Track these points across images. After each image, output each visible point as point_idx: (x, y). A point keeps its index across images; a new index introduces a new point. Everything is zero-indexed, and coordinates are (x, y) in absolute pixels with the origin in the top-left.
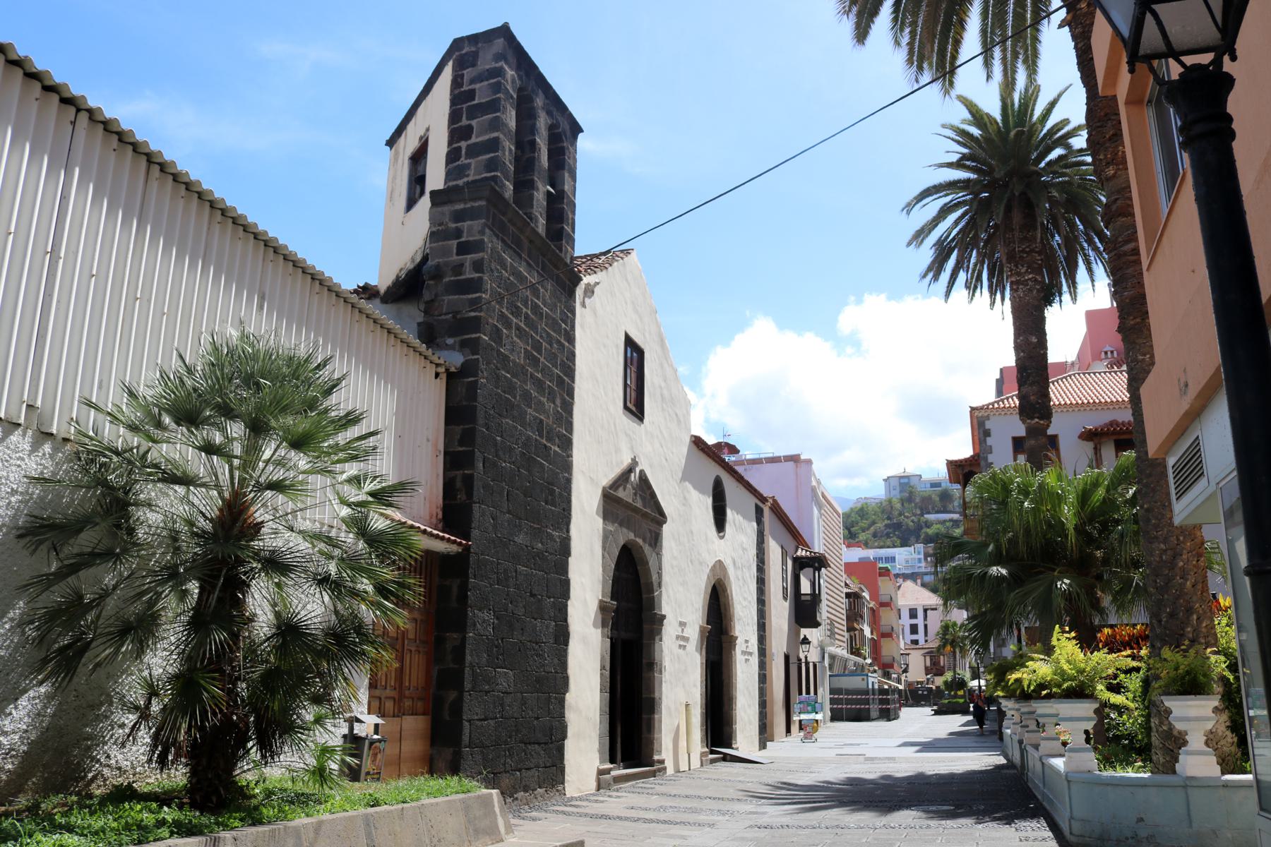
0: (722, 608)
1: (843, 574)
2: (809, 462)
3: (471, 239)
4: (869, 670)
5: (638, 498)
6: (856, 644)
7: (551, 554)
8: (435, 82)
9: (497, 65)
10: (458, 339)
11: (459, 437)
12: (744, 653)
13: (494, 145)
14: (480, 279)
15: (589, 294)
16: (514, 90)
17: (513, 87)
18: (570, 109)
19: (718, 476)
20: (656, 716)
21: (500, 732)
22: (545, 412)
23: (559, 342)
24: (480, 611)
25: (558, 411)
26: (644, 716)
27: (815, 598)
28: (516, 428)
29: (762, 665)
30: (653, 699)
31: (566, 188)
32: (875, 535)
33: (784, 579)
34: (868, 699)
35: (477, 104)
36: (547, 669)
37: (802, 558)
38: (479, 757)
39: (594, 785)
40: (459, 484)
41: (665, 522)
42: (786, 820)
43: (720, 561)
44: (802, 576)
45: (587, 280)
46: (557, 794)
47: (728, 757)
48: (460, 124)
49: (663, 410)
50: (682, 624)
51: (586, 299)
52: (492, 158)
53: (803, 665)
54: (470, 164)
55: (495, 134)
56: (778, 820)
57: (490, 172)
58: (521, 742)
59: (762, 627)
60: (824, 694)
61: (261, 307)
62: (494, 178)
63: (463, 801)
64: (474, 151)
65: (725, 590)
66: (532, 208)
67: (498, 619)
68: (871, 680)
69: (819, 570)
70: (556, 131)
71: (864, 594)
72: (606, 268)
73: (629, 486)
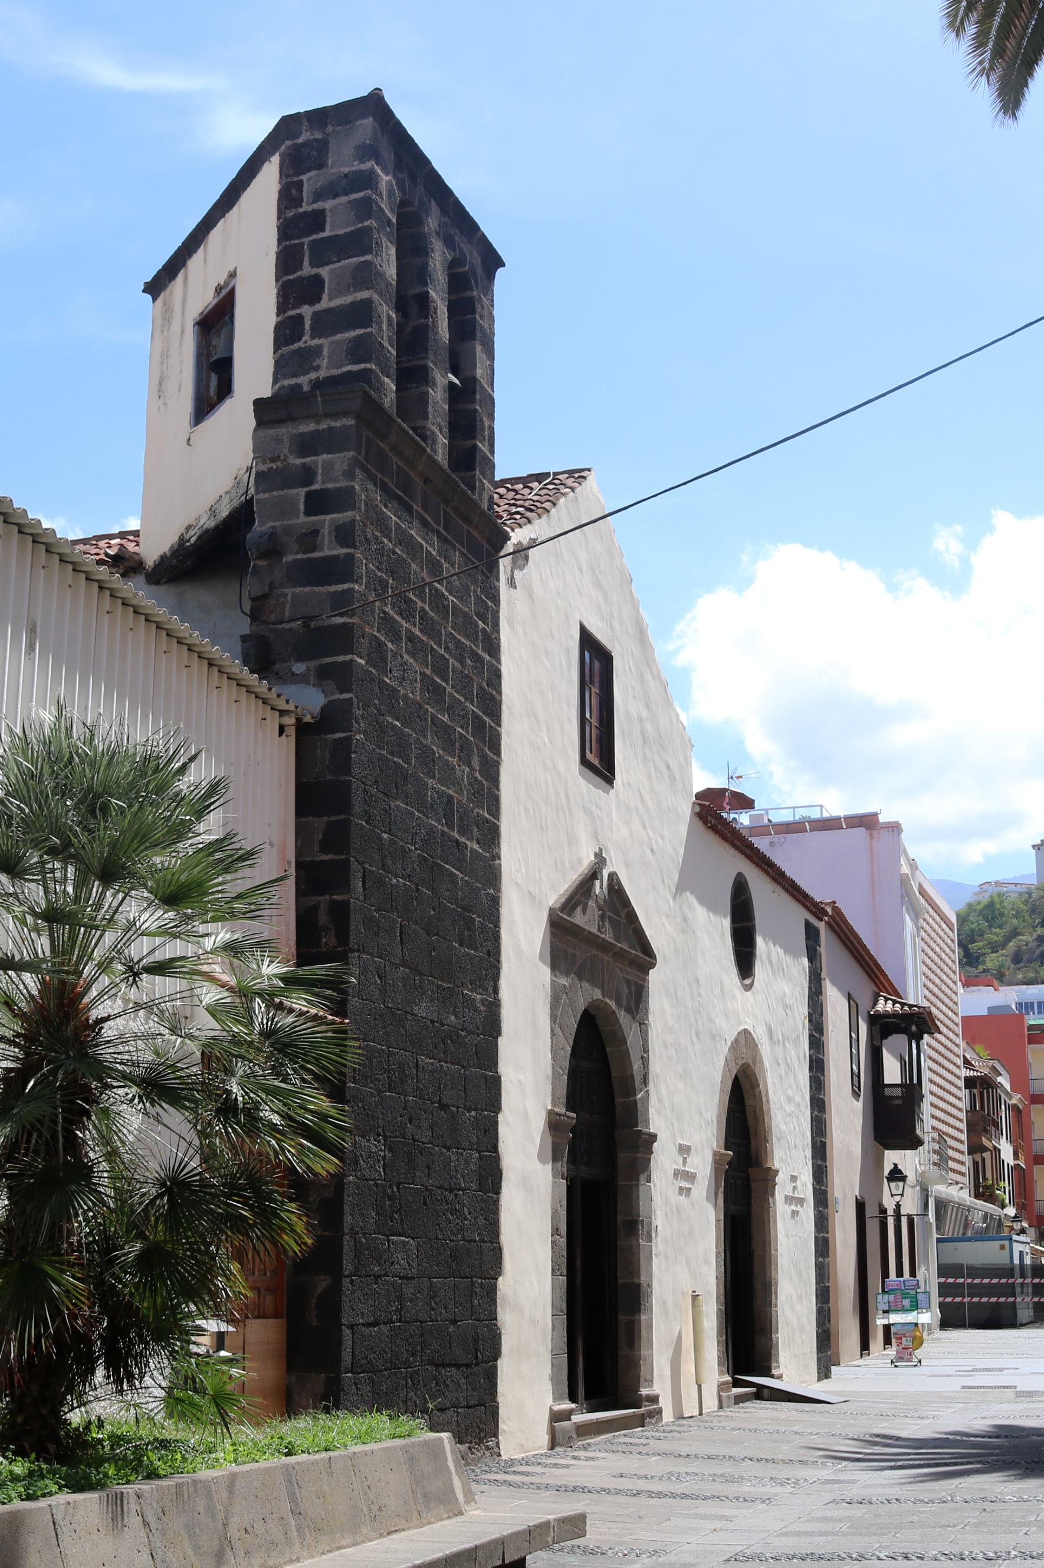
0: (750, 1117)
1: (959, 1041)
2: (895, 828)
3: (330, 486)
4: (1012, 1228)
5: (607, 924)
6: (985, 1179)
7: (470, 1033)
8: (244, 189)
9: (363, 167)
10: (314, 663)
11: (320, 836)
12: (789, 1200)
13: (362, 313)
14: (350, 557)
15: (520, 562)
16: (392, 210)
17: (390, 204)
18: (482, 229)
19: (740, 875)
20: (643, 1317)
21: (397, 1346)
22: (456, 782)
23: (475, 656)
24: (364, 1137)
25: (476, 779)
26: (622, 1318)
27: (912, 1091)
28: (412, 813)
29: (822, 1223)
30: (638, 1286)
31: (479, 372)
32: (1017, 959)
33: (854, 1058)
34: (1013, 1285)
36: (469, 1235)
37: (886, 1015)
38: (366, 1389)
39: (545, 1439)
40: (323, 918)
41: (653, 966)
42: (893, 1492)
43: (746, 1031)
44: (884, 1051)
45: (518, 536)
46: (488, 1454)
47: (766, 1392)
48: (299, 274)
49: (645, 758)
50: (684, 1150)
51: (516, 572)
52: (360, 336)
53: (891, 1222)
54: (320, 348)
55: (365, 295)
56: (879, 1491)
57: (359, 363)
58: (431, 1362)
59: (820, 1151)
60: (928, 1276)
61: (31, 647)
62: (365, 376)
63: (405, 1449)
64: (325, 324)
65: (754, 1084)
66: (426, 418)
67: (391, 1150)
68: (1017, 1248)
69: (919, 1038)
70: (460, 270)
71: (999, 1079)
72: (548, 511)
73: (591, 903)
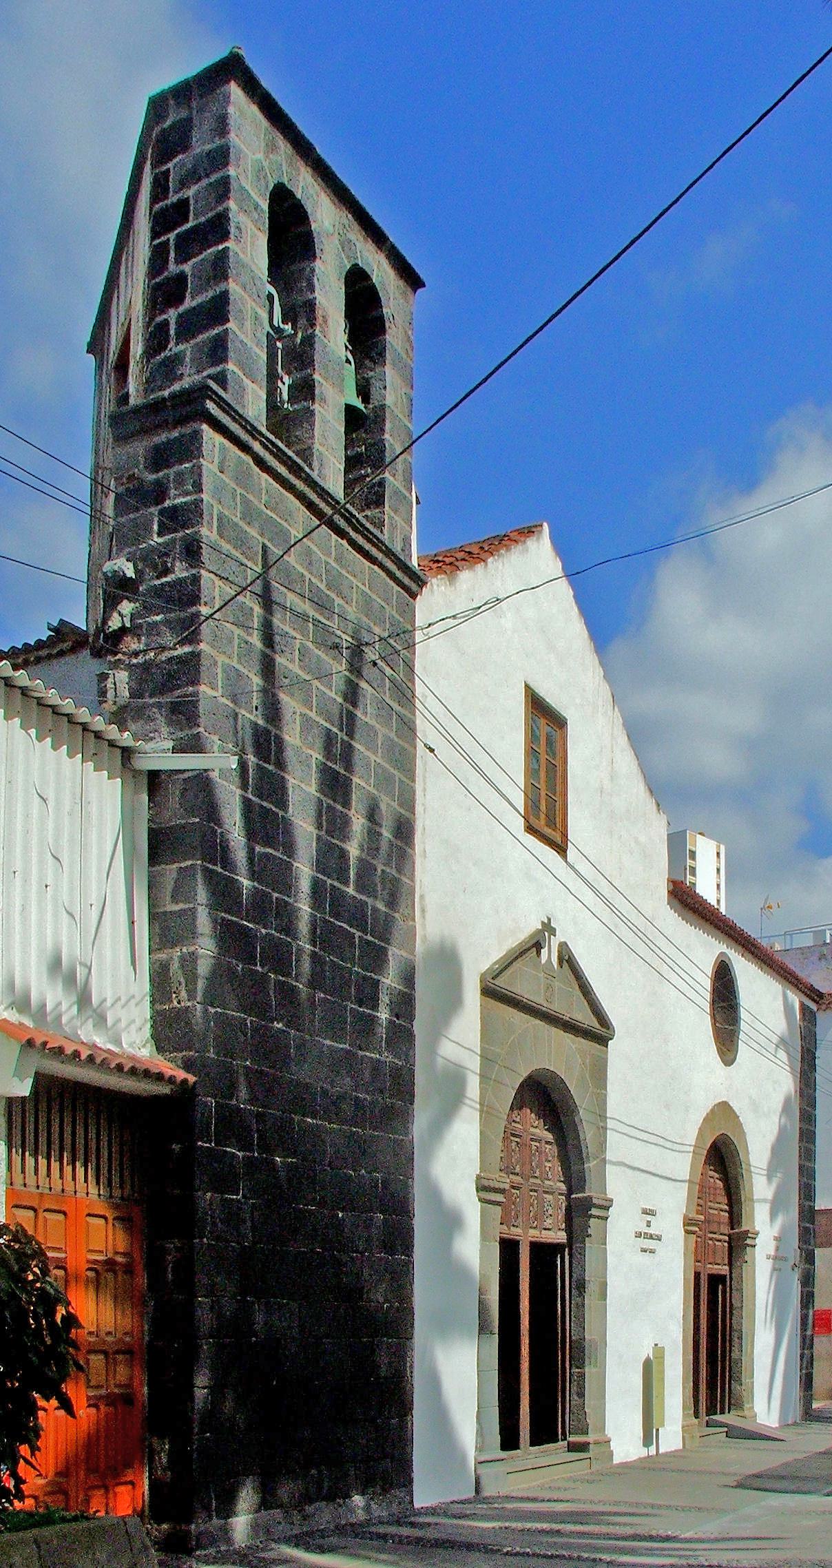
35: (192, 228)
